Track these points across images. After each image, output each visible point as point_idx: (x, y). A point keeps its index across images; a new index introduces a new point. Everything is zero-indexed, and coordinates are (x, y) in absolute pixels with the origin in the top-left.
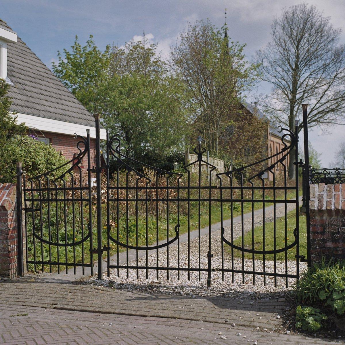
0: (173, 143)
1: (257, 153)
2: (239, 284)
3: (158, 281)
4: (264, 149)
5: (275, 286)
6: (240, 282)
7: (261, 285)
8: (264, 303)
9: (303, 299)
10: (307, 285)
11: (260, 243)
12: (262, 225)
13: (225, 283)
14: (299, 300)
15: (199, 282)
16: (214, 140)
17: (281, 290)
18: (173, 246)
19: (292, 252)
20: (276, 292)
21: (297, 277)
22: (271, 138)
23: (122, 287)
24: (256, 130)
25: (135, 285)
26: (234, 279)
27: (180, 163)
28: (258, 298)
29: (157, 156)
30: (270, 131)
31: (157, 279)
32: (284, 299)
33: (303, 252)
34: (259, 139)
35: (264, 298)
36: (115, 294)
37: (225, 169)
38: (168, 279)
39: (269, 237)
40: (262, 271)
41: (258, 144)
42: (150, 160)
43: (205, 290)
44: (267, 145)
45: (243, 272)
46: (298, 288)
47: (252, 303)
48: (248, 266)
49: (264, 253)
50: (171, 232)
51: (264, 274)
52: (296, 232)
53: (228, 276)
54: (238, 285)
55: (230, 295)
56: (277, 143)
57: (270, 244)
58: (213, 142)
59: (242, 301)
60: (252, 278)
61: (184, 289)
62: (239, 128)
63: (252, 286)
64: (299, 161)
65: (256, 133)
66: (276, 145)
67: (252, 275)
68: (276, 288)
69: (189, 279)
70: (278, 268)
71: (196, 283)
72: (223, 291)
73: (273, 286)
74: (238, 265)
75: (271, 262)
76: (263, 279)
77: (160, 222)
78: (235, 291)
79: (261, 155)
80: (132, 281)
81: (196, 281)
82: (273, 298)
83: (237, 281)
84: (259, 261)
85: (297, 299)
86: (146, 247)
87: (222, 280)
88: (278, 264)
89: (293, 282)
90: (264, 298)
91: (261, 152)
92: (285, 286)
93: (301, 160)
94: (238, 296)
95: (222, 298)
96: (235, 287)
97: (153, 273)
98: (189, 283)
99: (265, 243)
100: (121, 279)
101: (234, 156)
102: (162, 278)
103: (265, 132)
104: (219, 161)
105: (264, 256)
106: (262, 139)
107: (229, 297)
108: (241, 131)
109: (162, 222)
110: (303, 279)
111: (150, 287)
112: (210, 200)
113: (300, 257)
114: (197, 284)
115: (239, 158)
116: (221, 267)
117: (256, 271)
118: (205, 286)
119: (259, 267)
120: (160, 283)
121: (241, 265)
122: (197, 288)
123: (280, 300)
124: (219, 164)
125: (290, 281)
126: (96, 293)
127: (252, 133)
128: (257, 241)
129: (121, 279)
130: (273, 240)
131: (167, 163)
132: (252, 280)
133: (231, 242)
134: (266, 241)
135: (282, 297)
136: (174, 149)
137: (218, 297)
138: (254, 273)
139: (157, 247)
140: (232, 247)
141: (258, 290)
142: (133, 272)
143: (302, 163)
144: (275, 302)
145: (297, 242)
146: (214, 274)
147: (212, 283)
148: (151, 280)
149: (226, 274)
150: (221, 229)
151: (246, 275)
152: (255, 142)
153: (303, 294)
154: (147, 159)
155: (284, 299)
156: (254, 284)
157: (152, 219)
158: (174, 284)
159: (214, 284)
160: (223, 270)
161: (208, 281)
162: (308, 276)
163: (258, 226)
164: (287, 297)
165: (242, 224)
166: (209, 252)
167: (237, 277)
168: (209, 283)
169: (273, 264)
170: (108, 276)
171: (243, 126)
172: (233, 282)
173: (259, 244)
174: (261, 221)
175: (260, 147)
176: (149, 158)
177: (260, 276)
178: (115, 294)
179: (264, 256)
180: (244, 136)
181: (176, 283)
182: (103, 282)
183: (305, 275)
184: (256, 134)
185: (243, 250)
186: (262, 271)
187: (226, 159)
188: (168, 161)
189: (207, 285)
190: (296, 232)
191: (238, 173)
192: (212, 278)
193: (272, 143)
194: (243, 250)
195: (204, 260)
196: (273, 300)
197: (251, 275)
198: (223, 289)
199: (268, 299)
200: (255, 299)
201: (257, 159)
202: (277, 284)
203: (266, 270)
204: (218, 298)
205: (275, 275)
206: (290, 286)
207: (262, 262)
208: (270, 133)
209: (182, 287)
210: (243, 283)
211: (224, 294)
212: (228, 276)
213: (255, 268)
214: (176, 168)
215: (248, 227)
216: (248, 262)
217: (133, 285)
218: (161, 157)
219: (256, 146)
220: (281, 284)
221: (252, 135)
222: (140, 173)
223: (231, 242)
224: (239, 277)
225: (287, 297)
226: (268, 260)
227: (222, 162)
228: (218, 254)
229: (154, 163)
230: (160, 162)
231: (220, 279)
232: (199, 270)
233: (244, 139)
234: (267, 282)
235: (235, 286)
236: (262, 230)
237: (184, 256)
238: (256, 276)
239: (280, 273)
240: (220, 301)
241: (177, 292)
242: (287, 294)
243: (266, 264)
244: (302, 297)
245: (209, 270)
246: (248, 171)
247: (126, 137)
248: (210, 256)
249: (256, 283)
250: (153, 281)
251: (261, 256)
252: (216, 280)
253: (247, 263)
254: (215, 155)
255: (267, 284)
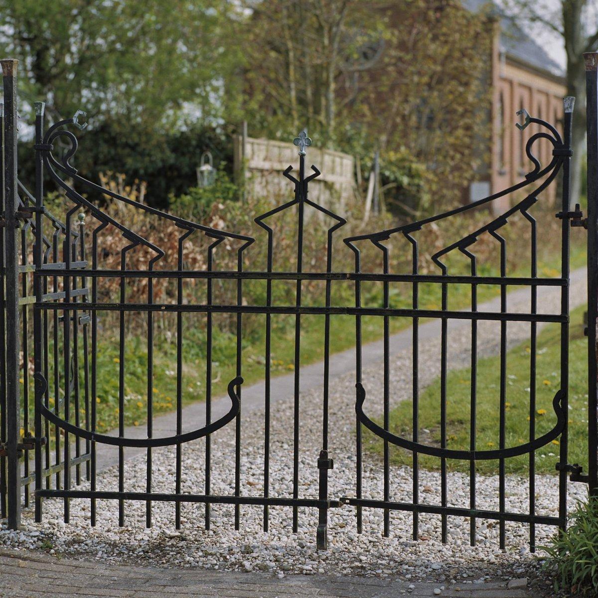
0: (191, 91)
1: (456, 128)
2: (403, 540)
3: (177, 534)
4: (481, 115)
5: (502, 546)
6: (407, 536)
7: (463, 543)
8: (472, 591)
9: (574, 580)
10: (586, 545)
11: (461, 422)
12: (468, 365)
13: (363, 538)
14: (563, 583)
15: (293, 536)
16: (320, 85)
17: (518, 557)
18: (224, 437)
19: (549, 454)
20: (502, 564)
21: (560, 522)
22: (503, 70)
23: (76, 549)
24: (457, 54)
25: (114, 545)
26: (391, 528)
27: (216, 166)
28: (455, 578)
29: (139, 134)
30: (499, 46)
31: (178, 527)
32: (524, 581)
33: (579, 453)
34: (466, 84)
35: (470, 577)
36: (61, 568)
37: (356, 181)
38: (207, 527)
39: (488, 406)
40: (467, 506)
41: (460, 100)
42: (112, 146)
43: (310, 557)
44: (491, 104)
45: (416, 508)
46: (561, 550)
47: (437, 591)
48: (427, 491)
49: (473, 455)
50: (195, 385)
51: (472, 514)
52: (561, 400)
53: (372, 518)
54: (401, 544)
55: (380, 571)
56: (522, 85)
57: (491, 427)
58: (316, 94)
59: (412, 586)
60: (440, 524)
61: (254, 555)
62: (402, 46)
63: (439, 545)
64: (572, 208)
65: (455, 64)
66: (518, 91)
67: (440, 516)
68: (504, 552)
69: (266, 530)
70: (512, 498)
71: (284, 539)
72: (361, 561)
73: (496, 548)
74: (402, 491)
75: (491, 479)
76: (467, 526)
77: (161, 355)
78: (391, 558)
79: (471, 137)
80: (106, 534)
81: (283, 532)
82: (496, 578)
83: (398, 532)
84: (459, 475)
85: (559, 580)
86: (147, 438)
87: (355, 530)
88: (512, 484)
89: (551, 536)
90: (470, 577)
91: (468, 128)
92: (527, 548)
93: (577, 206)
94: (399, 574)
95: (356, 579)
96: (391, 549)
97: (163, 512)
98: (266, 538)
99: (477, 422)
100: (73, 529)
101: (384, 138)
102: (188, 525)
103: (485, 62)
104: (338, 160)
105: (472, 465)
106: (475, 85)
107: (377, 576)
108: (408, 57)
109: (166, 353)
110: (574, 529)
111: (158, 549)
112: (299, 276)
113: (569, 468)
114: (288, 540)
115: (398, 146)
116: (352, 494)
117: (449, 505)
118: (309, 548)
119: (459, 498)
120: (183, 539)
121: (410, 487)
122: (289, 552)
123: (514, 583)
124: (338, 169)
125: (544, 534)
126: (8, 569)
127: (443, 64)
128: (453, 417)
129: (73, 529)
130: (498, 414)
131: (171, 158)
132: (440, 530)
133: (382, 426)
134: (478, 416)
135: (520, 576)
136: (191, 111)
137: (346, 575)
138: (444, 511)
139: (179, 439)
140: (384, 438)
141: (453, 556)
142: (108, 510)
143: (581, 214)
144: (500, 588)
145: (562, 427)
146: (332, 513)
147: (330, 537)
148: (156, 532)
149: (366, 512)
150: (355, 389)
151: (422, 516)
152: (451, 92)
153: (574, 567)
154: (106, 141)
155: (524, 581)
156: (444, 541)
157: (139, 343)
158: (224, 540)
159: (335, 543)
160: (359, 503)
161: (318, 533)
162: (587, 519)
163: (459, 365)
164: (532, 576)
165: (409, 362)
166: (324, 454)
167: (395, 522)
168: (321, 537)
169: (497, 484)
170: (38, 519)
171: (416, 42)
172: (386, 534)
173: (459, 427)
174: (466, 350)
175: (466, 111)
176: (112, 141)
177: (459, 520)
178: (61, 568)
179: (472, 465)
180: (419, 73)
181: (228, 539)
182: (23, 538)
183: (580, 520)
184: (456, 68)
185: (415, 447)
186: (467, 506)
187: (359, 149)
188: (174, 150)
189: (315, 544)
190: (561, 400)
191: (397, 197)
192: (330, 524)
193: (506, 88)
194: (415, 447)
195: (309, 473)
196: (496, 585)
197: (435, 516)
198: (359, 554)
199: (481, 581)
200: (448, 580)
201: (456, 150)
202: (507, 542)
203: (478, 500)
204: (349, 579)
205: (502, 516)
206: (541, 548)
207: (468, 480)
208: (500, 55)
209: (247, 551)
210: (415, 539)
211: (362, 567)
212: (372, 518)
213: (449, 497)
214: (206, 183)
215: (430, 371)
216: (430, 480)
217: (110, 545)
218: (148, 135)
219: (455, 106)
220: (517, 540)
221: (443, 72)
222: (90, 195)
223: (382, 426)
224: (402, 520)
225: (532, 576)
226: (485, 474)
227: (348, 162)
228: (341, 456)
229: (129, 155)
230: (149, 155)
231: (349, 528)
232: (295, 503)
233: (418, 84)
234: (478, 537)
235: (392, 547)
236: (469, 383)
237: (252, 465)
238: (451, 518)
239: (516, 511)
240: (351, 588)
241: (233, 564)
242: (531, 569)
243: (477, 486)
244: (570, 576)
245: (323, 504)
246: (426, 187)
247: (38, 67)
248: (325, 464)
249: (449, 538)
250: (164, 533)
251: (465, 463)
252: (340, 530)
253: (425, 482)
254: (324, 133)
255: (480, 541)
